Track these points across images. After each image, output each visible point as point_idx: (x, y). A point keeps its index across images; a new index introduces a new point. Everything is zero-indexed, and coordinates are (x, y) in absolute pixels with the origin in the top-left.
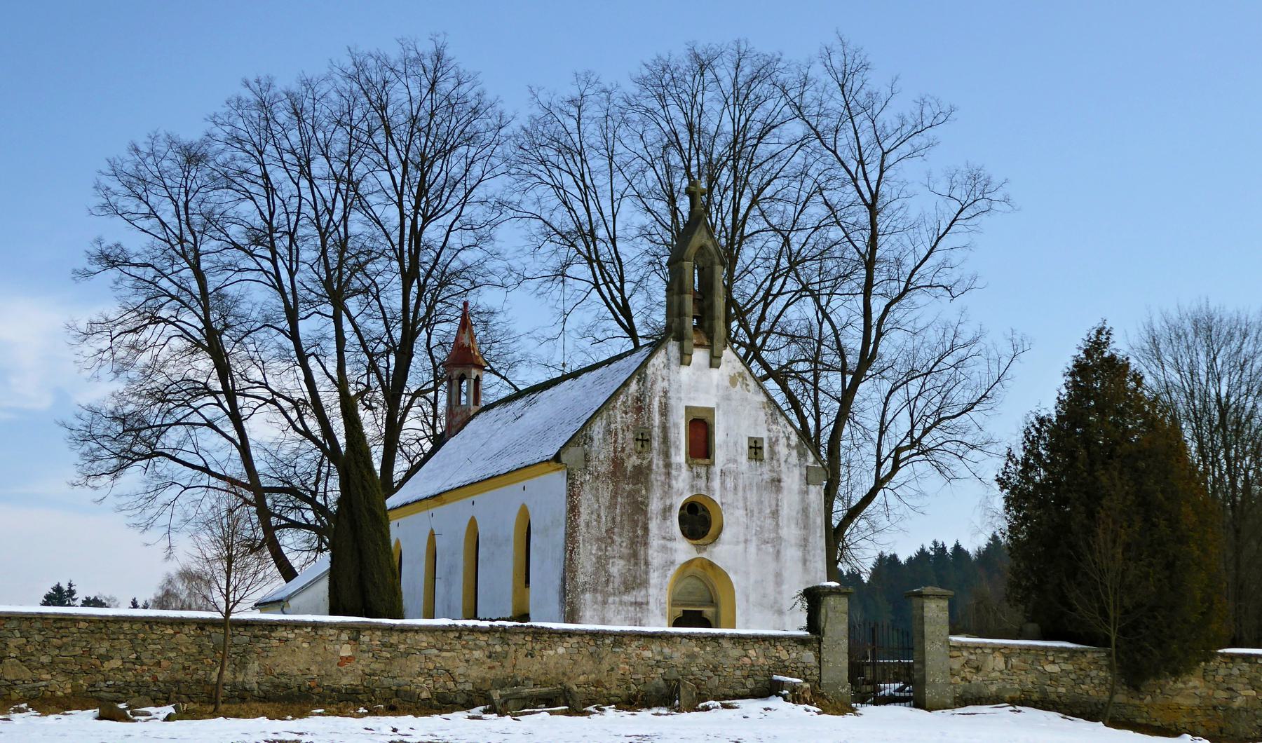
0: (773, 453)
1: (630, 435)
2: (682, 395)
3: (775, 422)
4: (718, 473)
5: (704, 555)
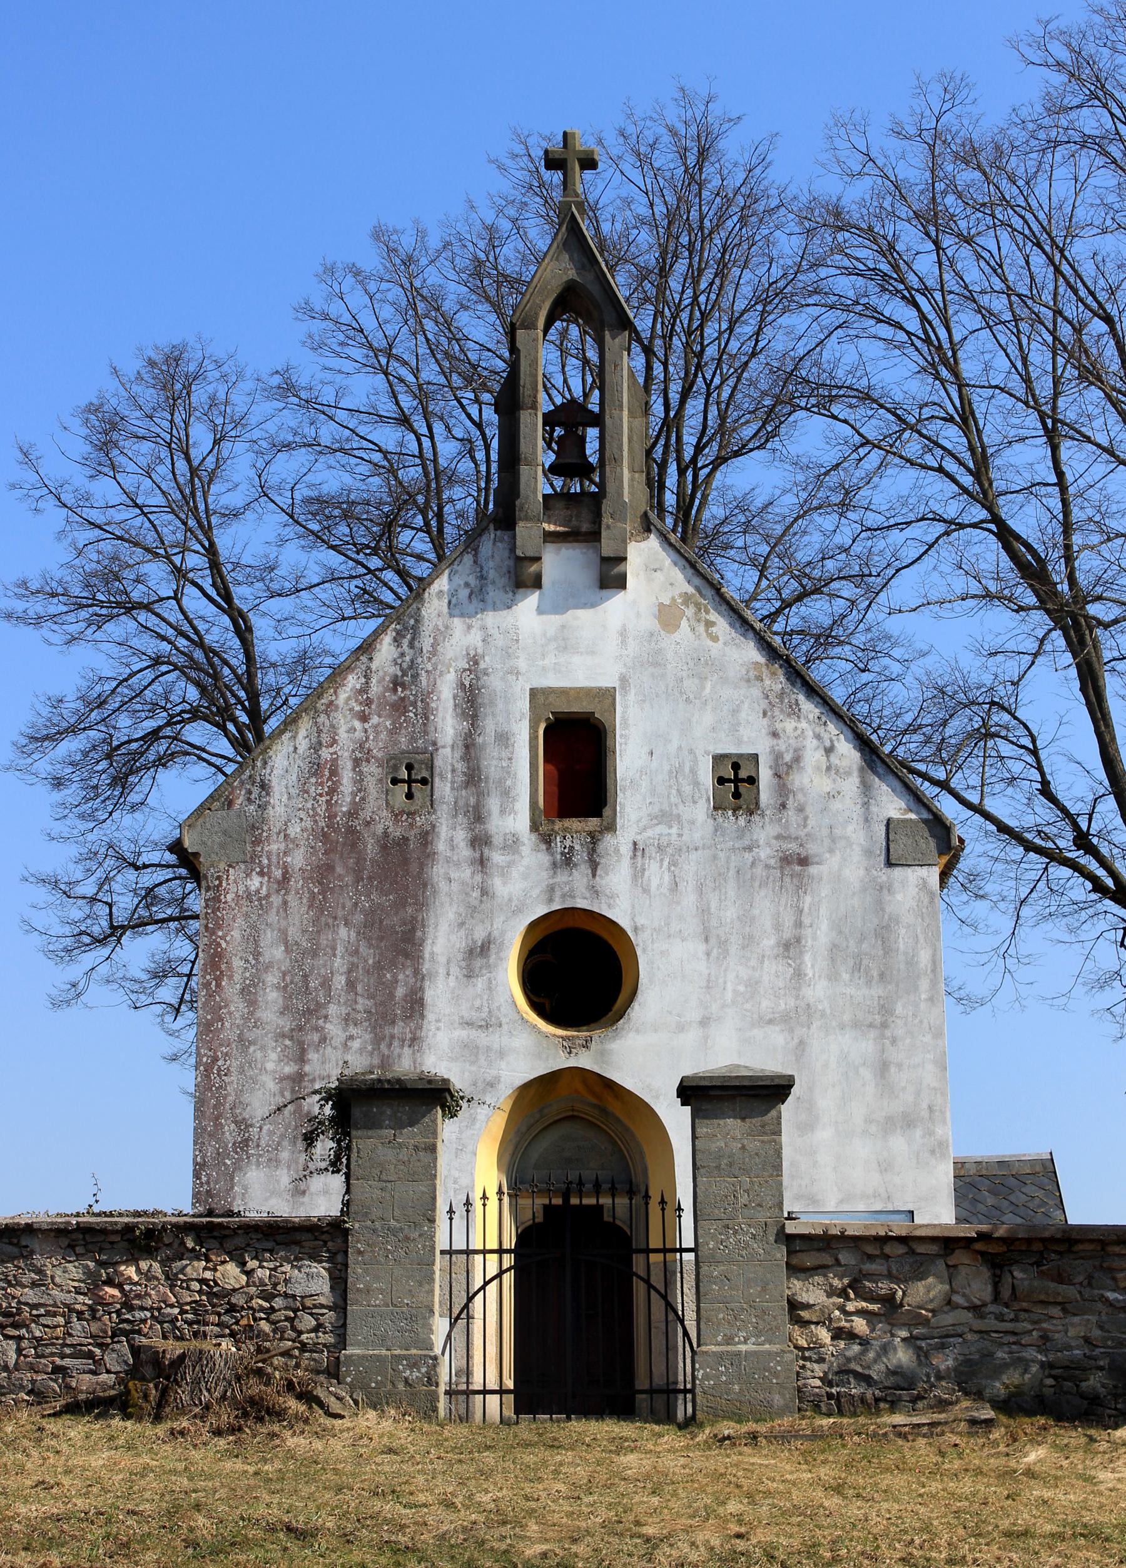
0: (783, 790)
1: (372, 770)
2: (522, 664)
3: (794, 711)
4: (626, 849)
5: (584, 1060)
